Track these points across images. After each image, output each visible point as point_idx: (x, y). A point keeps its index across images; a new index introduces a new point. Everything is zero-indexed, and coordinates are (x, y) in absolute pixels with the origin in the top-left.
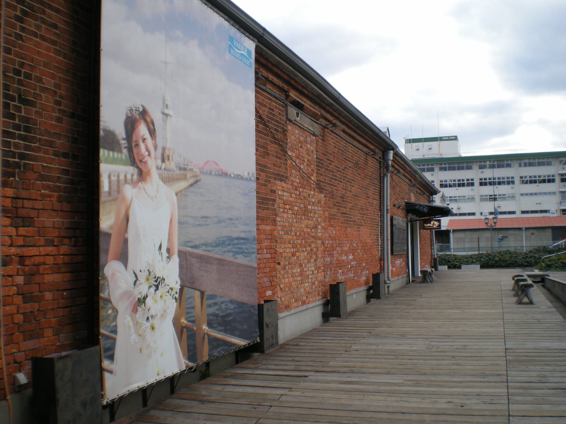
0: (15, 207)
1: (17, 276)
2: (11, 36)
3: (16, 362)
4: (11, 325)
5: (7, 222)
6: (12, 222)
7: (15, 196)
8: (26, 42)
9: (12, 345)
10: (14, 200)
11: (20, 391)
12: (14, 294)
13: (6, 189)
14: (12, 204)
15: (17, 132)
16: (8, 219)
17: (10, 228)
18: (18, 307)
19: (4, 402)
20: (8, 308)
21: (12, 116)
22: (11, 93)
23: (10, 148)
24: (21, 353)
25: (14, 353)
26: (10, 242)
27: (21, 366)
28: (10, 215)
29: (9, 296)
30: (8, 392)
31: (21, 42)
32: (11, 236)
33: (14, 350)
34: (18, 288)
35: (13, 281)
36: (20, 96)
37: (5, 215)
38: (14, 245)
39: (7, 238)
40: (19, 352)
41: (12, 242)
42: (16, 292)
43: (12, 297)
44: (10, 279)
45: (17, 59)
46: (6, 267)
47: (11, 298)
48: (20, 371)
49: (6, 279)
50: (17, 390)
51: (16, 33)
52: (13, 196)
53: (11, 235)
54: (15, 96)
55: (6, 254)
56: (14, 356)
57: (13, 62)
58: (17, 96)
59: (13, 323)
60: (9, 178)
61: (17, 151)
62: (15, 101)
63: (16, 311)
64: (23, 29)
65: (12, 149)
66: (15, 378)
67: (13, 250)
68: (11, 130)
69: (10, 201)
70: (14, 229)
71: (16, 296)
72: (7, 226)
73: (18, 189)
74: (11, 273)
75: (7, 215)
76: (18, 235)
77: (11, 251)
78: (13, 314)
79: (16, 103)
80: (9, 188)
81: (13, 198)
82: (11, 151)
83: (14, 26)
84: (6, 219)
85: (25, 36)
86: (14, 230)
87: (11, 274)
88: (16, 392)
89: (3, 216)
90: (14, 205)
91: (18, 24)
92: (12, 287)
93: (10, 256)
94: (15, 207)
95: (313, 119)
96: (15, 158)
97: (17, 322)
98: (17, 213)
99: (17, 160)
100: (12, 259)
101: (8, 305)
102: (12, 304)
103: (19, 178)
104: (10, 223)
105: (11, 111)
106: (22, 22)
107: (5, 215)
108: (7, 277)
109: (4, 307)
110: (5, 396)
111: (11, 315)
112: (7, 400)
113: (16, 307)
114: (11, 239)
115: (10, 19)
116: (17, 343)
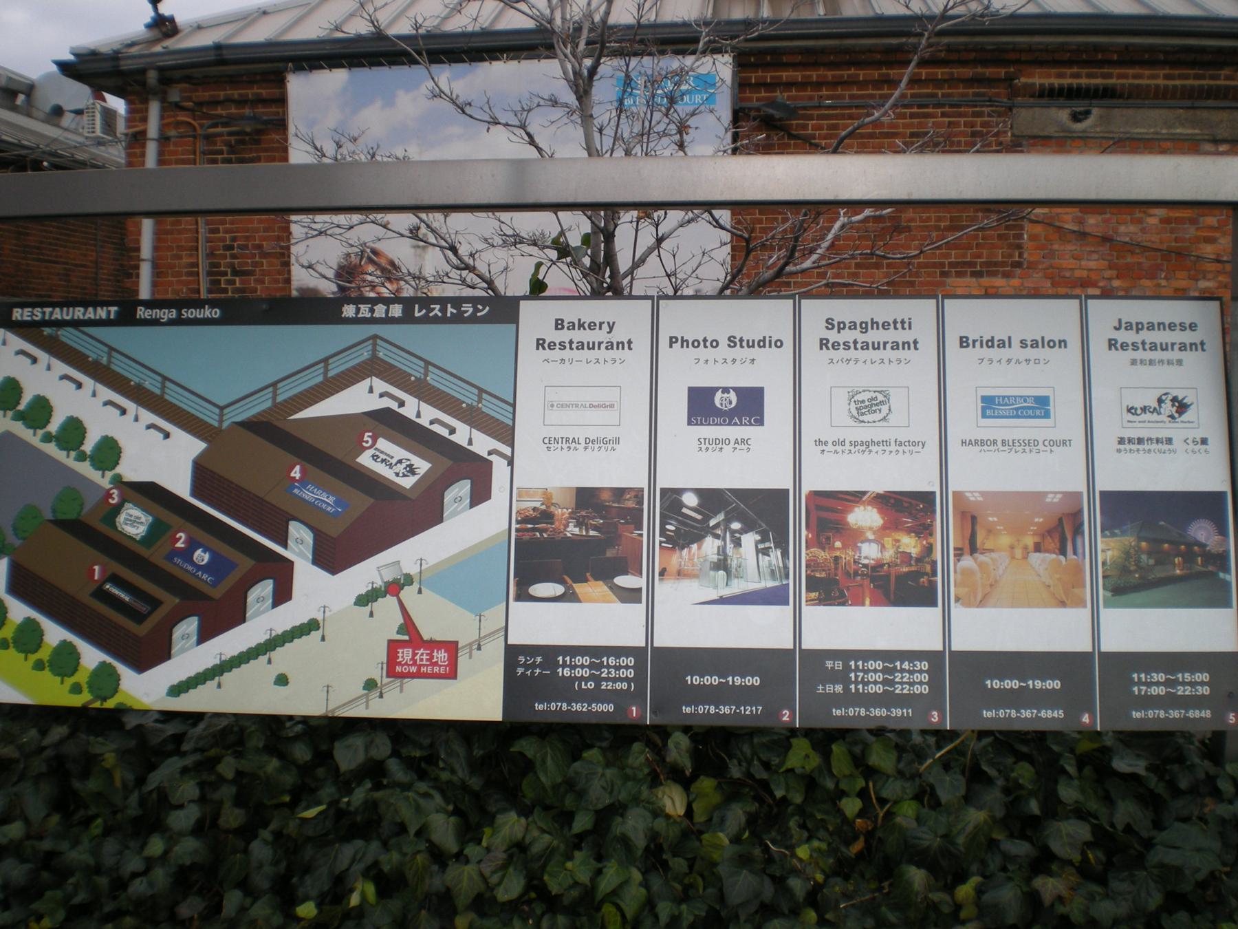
45: (227, 236)
79: (229, 277)
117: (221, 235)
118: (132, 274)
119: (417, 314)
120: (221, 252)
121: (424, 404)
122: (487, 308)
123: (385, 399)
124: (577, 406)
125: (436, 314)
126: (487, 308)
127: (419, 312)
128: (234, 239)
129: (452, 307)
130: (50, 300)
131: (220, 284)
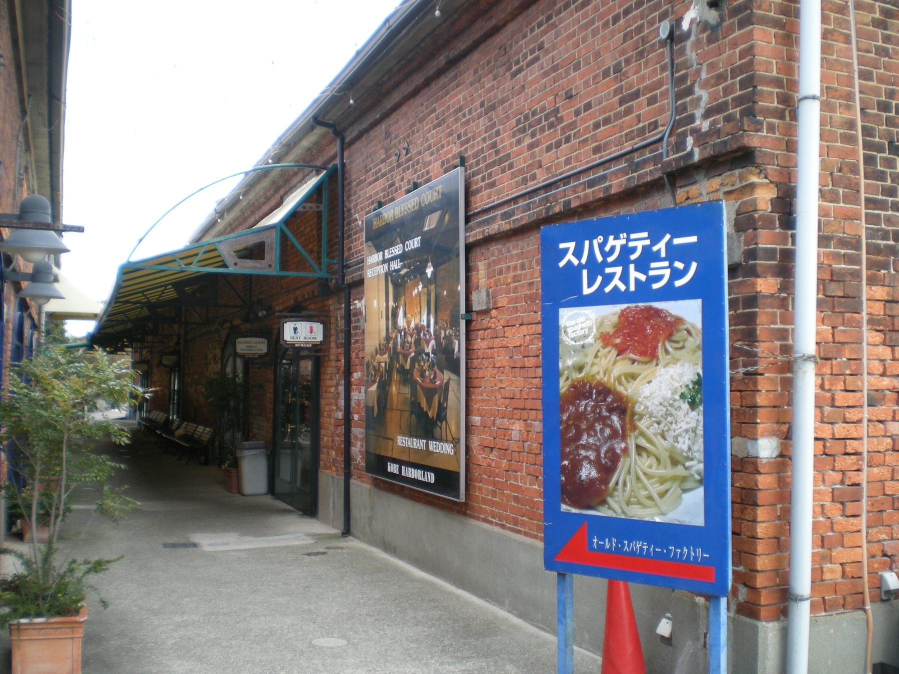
0: (889, 316)
1: (891, 423)
2: (869, 52)
3: (885, 555)
4: (881, 497)
5: (878, 338)
6: (885, 339)
7: (891, 298)
8: (895, 57)
9: (882, 528)
10: (887, 304)
11: (888, 600)
12: (887, 450)
13: (873, 288)
14: (885, 312)
15: (890, 199)
16: (878, 333)
17: (881, 349)
18: (893, 470)
19: (860, 612)
20: (875, 470)
21: (881, 176)
22: (877, 139)
23: (881, 225)
24: (893, 541)
25: (885, 540)
26: (881, 370)
27: (893, 561)
28: (881, 328)
29: (879, 452)
30: (868, 599)
31: (886, 59)
32: (884, 360)
33: (884, 536)
34: (893, 440)
35: (886, 430)
36: (891, 143)
37: (874, 327)
38: (888, 374)
39: (877, 363)
40: (892, 539)
41: (885, 369)
42: (890, 447)
43: (885, 454)
44: (881, 426)
45: (883, 87)
46: (876, 408)
47: (882, 455)
48: (891, 569)
49: (875, 426)
50: (884, 597)
51: (877, 47)
52: (886, 298)
53: (883, 358)
54: (883, 144)
55: (875, 388)
56: (883, 545)
57: (876, 91)
58: (887, 143)
59: (885, 495)
60: (879, 271)
61: (891, 228)
62: (884, 152)
63: (888, 476)
64: (887, 39)
65: (883, 226)
66: (881, 579)
67: (886, 382)
68: (880, 197)
69: (882, 306)
70: (890, 349)
71: (890, 452)
72: (878, 345)
73: (844, 281)
74: (882, 418)
75: (878, 328)
76: (894, 359)
77: (884, 383)
78: (886, 480)
79: (886, 155)
80: (880, 287)
81: (887, 301)
82: (881, 230)
83: (872, 37)
84: (875, 333)
85: (893, 49)
86: (888, 350)
87: (884, 419)
88: (882, 600)
89: (871, 329)
90: (888, 312)
91: (880, 32)
92: (884, 439)
93: (883, 390)
94: (889, 316)
95: (388, 104)
96: (889, 240)
97: (890, 493)
98: (893, 325)
99: (891, 242)
100: (885, 396)
101: (878, 466)
102: (884, 465)
103: (894, 270)
104: (882, 340)
105: (879, 168)
106: (885, 28)
107: (874, 327)
108: (877, 423)
109: (870, 469)
110: (863, 603)
111: (881, 481)
112: (865, 610)
113: (890, 470)
114: (884, 365)
115: (866, 27)
116: (889, 526)
117: (874, 83)
118: (761, 123)
119: (587, 291)
120: (876, 111)
121: (633, 584)
122: (694, 265)
123: (855, 418)
124: (566, 640)
125: (616, 288)
126: (694, 265)
127: (590, 284)
128: (891, 94)
129: (636, 270)
130: (576, 171)
131: (876, 165)
